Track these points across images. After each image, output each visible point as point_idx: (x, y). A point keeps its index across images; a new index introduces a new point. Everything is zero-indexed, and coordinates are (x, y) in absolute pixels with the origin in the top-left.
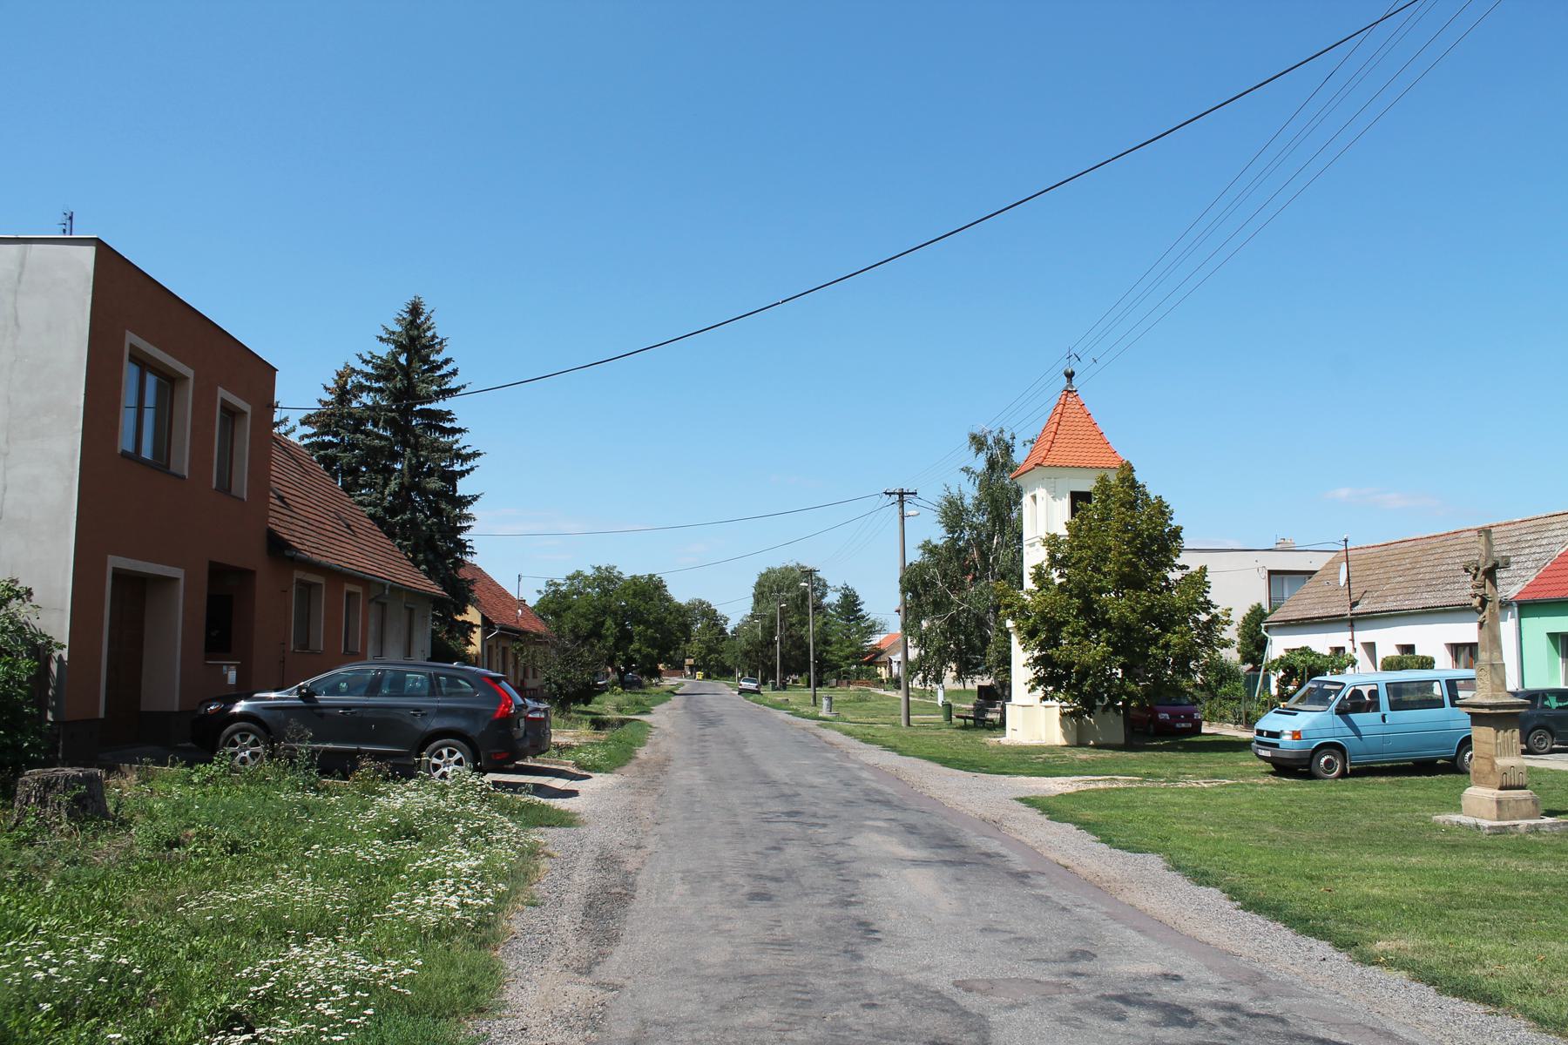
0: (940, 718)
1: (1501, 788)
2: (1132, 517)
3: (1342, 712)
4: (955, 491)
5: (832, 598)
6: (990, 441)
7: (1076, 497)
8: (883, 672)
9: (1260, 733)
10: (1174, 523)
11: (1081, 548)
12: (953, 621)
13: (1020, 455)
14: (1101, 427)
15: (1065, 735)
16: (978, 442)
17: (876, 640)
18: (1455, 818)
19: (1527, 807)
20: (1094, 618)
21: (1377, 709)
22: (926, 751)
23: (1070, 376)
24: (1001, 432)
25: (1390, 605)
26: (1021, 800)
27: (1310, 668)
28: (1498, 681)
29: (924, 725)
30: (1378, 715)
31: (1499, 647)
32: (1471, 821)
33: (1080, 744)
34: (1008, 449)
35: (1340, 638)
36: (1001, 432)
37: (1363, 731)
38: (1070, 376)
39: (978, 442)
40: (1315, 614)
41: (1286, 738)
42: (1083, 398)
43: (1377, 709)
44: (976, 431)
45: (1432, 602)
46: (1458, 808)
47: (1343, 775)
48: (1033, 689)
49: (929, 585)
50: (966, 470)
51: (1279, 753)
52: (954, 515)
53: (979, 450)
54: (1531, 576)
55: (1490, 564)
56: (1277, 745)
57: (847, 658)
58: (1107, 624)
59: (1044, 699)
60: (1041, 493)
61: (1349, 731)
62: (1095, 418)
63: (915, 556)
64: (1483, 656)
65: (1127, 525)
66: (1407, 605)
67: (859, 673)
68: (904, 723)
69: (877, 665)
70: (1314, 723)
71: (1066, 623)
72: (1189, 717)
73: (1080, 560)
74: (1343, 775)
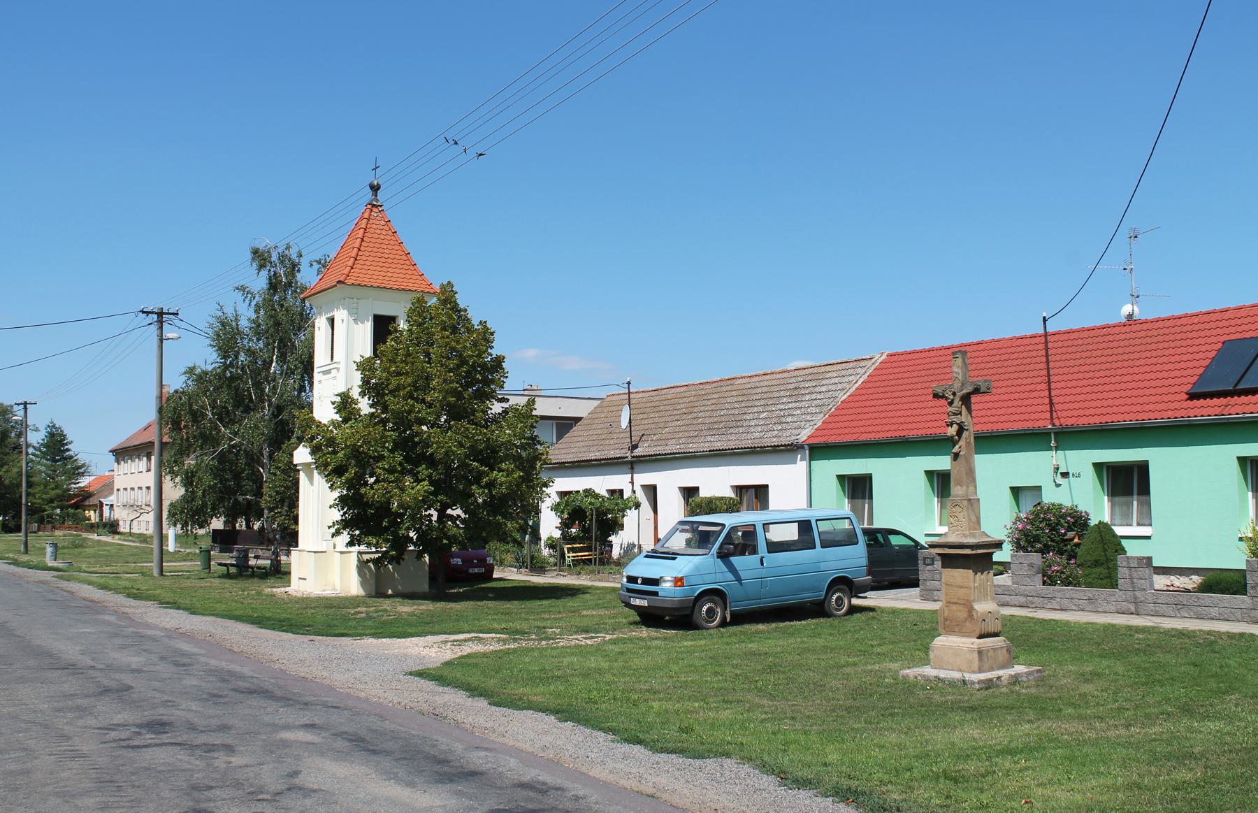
0: (197, 564)
1: (980, 637)
2: (458, 342)
3: (723, 555)
4: (230, 312)
5: (36, 438)
6: (274, 258)
7: (383, 326)
8: (93, 516)
9: (632, 579)
10: (495, 352)
11: (399, 374)
12: (222, 457)
13: (307, 276)
14: (408, 246)
15: (363, 584)
16: (260, 258)
17: (84, 482)
18: (929, 671)
19: (1002, 656)
20: (413, 454)
21: (754, 551)
22: (221, 607)
23: (375, 189)
24: (288, 248)
25: (672, 447)
26: (421, 674)
27: (597, 509)
28: (974, 519)
29: (178, 575)
30: (756, 558)
31: (974, 480)
32: (956, 675)
33: (380, 594)
34: (294, 268)
35: (619, 481)
36: (288, 248)
37: (743, 575)
38: (375, 189)
39: (260, 258)
40: (592, 456)
41: (667, 585)
42: (389, 215)
43: (754, 551)
44: (261, 246)
45: (718, 445)
46: (926, 662)
47: (723, 624)
48: (337, 533)
49: (196, 416)
50: (242, 289)
51: (656, 602)
52: (226, 338)
53: (261, 267)
54: (819, 420)
55: (969, 389)
56: (656, 594)
57: (51, 501)
58: (431, 462)
59: (351, 544)
60: (341, 315)
61: (730, 576)
62: (401, 236)
63: (176, 382)
64: (956, 490)
65: (453, 349)
66: (692, 448)
67: (63, 518)
68: (156, 572)
69: (85, 508)
70: (697, 568)
71: (382, 458)
72: (482, 561)
73: (398, 388)
74: (723, 624)
